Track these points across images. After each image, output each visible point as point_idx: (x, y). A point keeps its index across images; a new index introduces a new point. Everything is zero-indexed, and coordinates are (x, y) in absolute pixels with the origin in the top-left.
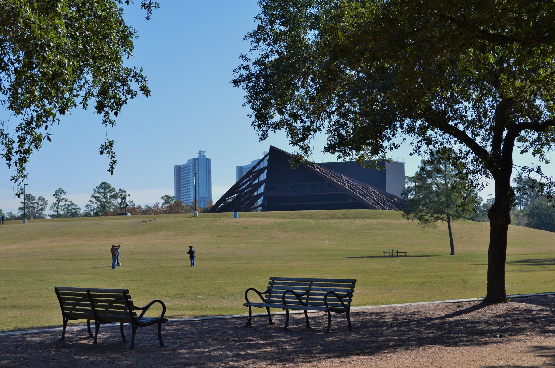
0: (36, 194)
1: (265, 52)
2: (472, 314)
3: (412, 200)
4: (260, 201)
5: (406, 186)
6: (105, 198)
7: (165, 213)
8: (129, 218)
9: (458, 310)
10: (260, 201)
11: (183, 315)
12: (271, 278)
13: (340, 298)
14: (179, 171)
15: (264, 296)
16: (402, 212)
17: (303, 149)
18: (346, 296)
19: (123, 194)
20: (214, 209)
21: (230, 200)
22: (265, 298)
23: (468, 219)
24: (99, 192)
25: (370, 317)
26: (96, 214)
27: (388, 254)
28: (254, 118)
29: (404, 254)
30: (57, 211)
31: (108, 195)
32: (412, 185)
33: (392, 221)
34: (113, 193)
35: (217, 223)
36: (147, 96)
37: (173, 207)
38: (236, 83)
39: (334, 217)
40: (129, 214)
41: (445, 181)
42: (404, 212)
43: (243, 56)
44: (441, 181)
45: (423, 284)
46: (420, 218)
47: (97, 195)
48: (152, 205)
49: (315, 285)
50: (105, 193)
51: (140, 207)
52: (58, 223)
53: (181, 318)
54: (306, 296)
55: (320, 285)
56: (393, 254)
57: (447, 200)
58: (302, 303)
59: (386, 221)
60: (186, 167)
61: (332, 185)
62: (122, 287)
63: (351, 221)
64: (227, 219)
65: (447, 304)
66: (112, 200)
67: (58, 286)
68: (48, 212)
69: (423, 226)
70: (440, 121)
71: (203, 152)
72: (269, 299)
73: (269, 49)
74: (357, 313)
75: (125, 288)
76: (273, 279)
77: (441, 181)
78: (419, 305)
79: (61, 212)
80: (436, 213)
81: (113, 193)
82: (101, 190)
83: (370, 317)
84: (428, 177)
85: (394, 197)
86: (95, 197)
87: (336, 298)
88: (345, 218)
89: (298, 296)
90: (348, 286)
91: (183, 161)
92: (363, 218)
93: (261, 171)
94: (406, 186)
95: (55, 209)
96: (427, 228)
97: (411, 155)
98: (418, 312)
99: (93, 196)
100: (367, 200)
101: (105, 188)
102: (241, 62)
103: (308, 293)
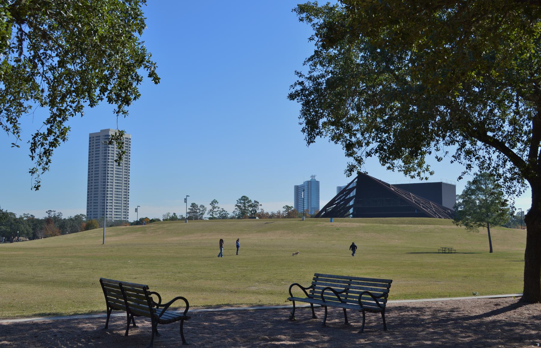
0: (199, 204)
1: (321, 73)
2: (509, 313)
3: (460, 211)
4: (351, 211)
5: (457, 202)
6: (245, 207)
7: (285, 217)
8: (257, 220)
9: (495, 309)
10: (351, 211)
11: (241, 304)
12: (315, 275)
13: (374, 297)
14: (298, 189)
15: (308, 291)
16: (453, 220)
17: (356, 160)
18: (382, 296)
19: (255, 205)
20: (318, 215)
21: (329, 209)
22: (309, 293)
23: (503, 226)
24: (241, 203)
25: (411, 313)
26: (239, 218)
27: (441, 251)
28: (304, 125)
29: (454, 251)
30: (212, 215)
31: (247, 205)
32: (461, 201)
33: (446, 227)
34: (250, 203)
35: (318, 225)
36: (156, 83)
37: (290, 214)
38: (292, 97)
39: (403, 223)
40: (257, 218)
41: (486, 197)
42: (455, 220)
43: (298, 73)
44: (482, 197)
45: (466, 277)
46: (466, 225)
47: (239, 205)
48: (275, 212)
49: (354, 283)
50: (244, 203)
51: (267, 213)
52: (213, 223)
53: (239, 307)
54: (345, 294)
55: (358, 283)
56: (446, 251)
57: (487, 212)
58: (340, 300)
59: (442, 226)
60: (302, 186)
61: (403, 200)
62: (144, 283)
63: (416, 226)
64: (326, 223)
65: (486, 300)
66: (249, 208)
67: (104, 277)
68: (206, 216)
69: (469, 230)
70: (478, 132)
71: (314, 177)
72: (313, 294)
73: (325, 70)
74: (400, 307)
75: (146, 284)
76: (317, 275)
77: (482, 197)
78: (459, 301)
79: (215, 216)
80: (478, 221)
81: (250, 203)
82: (242, 201)
83: (411, 313)
84: (472, 194)
85: (448, 209)
86: (238, 206)
87: (370, 297)
88: (411, 224)
89: (336, 293)
90: (384, 286)
91: (300, 183)
92: (424, 224)
93: (351, 190)
94: (457, 202)
95: (211, 213)
96: (471, 232)
97: (452, 162)
98: (457, 308)
99: (237, 205)
100: (428, 211)
101: (244, 200)
102: (297, 78)
103: (346, 291)
